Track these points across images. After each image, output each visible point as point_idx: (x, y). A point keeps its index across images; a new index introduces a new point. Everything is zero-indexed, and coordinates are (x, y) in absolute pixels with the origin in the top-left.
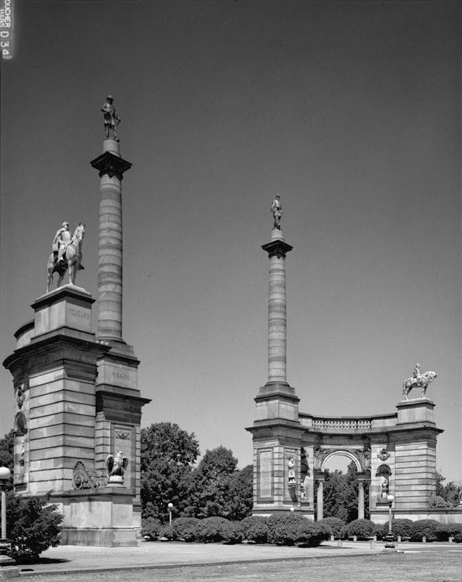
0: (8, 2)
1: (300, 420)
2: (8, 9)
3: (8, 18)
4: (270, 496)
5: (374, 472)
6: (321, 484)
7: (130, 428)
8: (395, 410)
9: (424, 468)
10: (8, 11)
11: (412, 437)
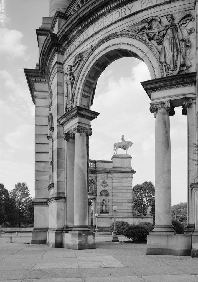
0: (3, 1)
2: (3, 4)
3: (3, 8)
5: (98, 194)
10: (3, 5)
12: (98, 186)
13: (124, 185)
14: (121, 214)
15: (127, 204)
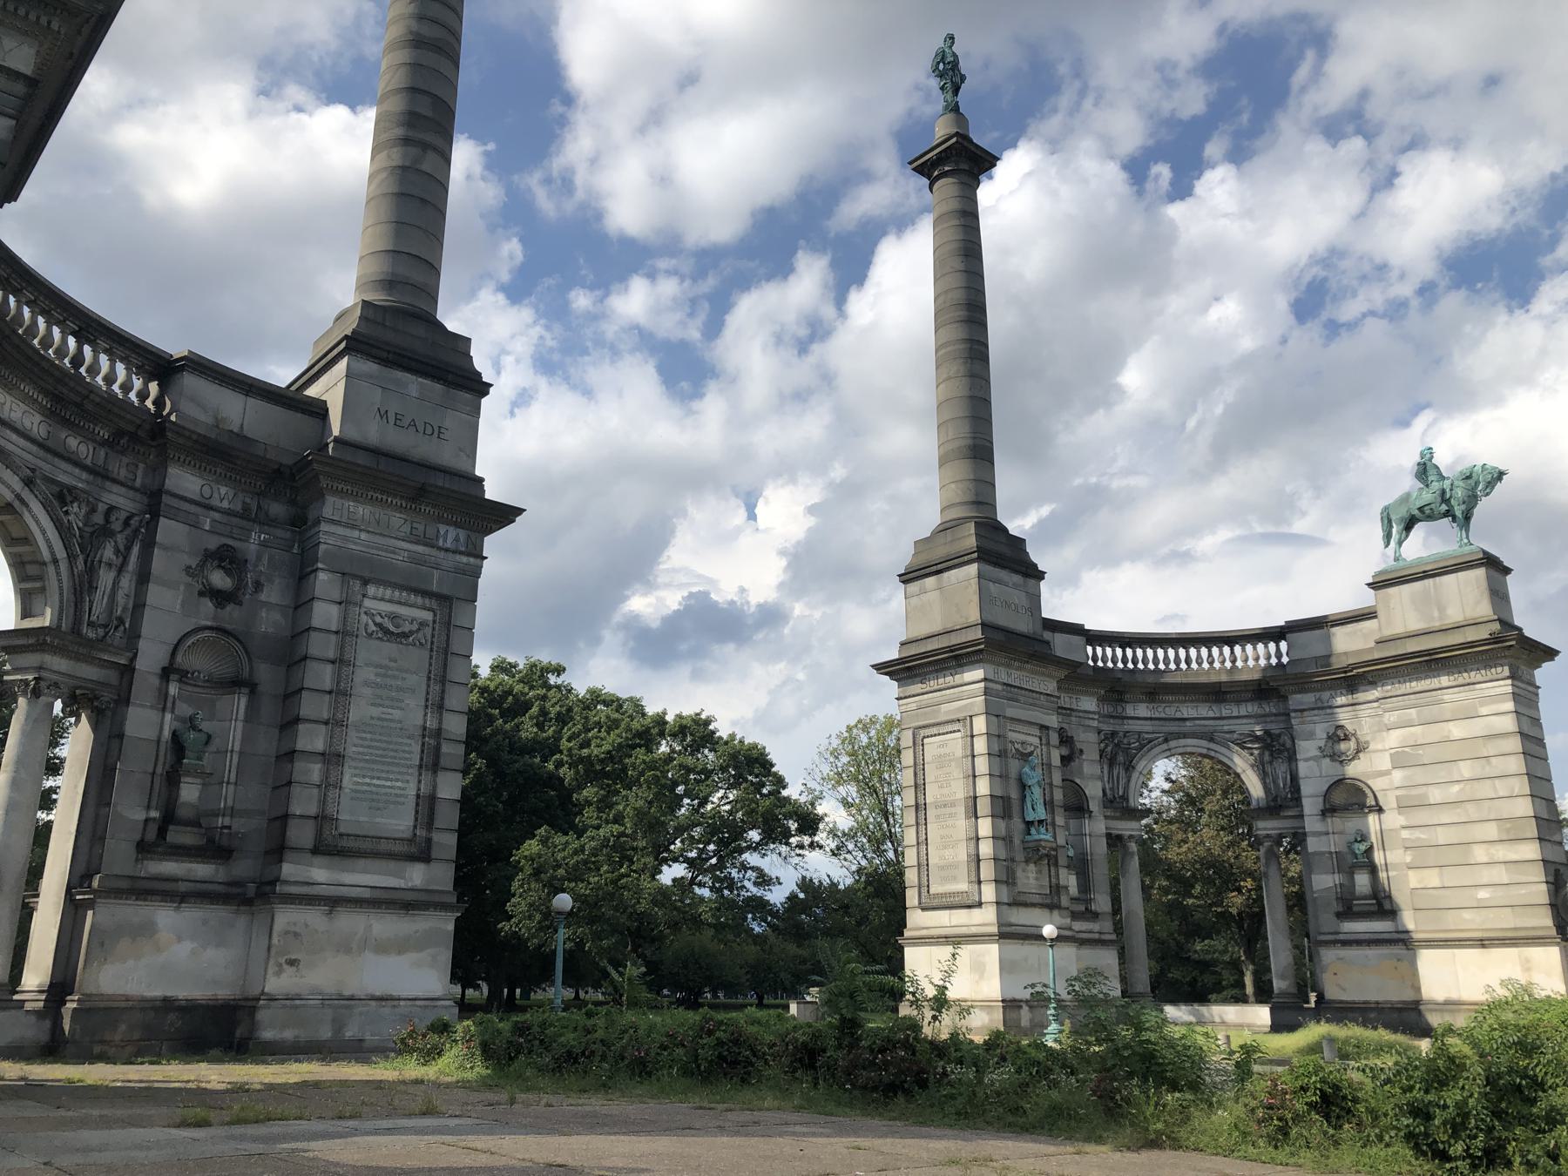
1: (1047, 635)
4: (963, 886)
5: (1311, 806)
6: (1133, 847)
7: (383, 716)
8: (1367, 599)
9: (1361, 700)
11: (74, 51)
12: (1306, 760)
13: (1457, 730)
14: (1467, 915)
15: (1499, 847)
